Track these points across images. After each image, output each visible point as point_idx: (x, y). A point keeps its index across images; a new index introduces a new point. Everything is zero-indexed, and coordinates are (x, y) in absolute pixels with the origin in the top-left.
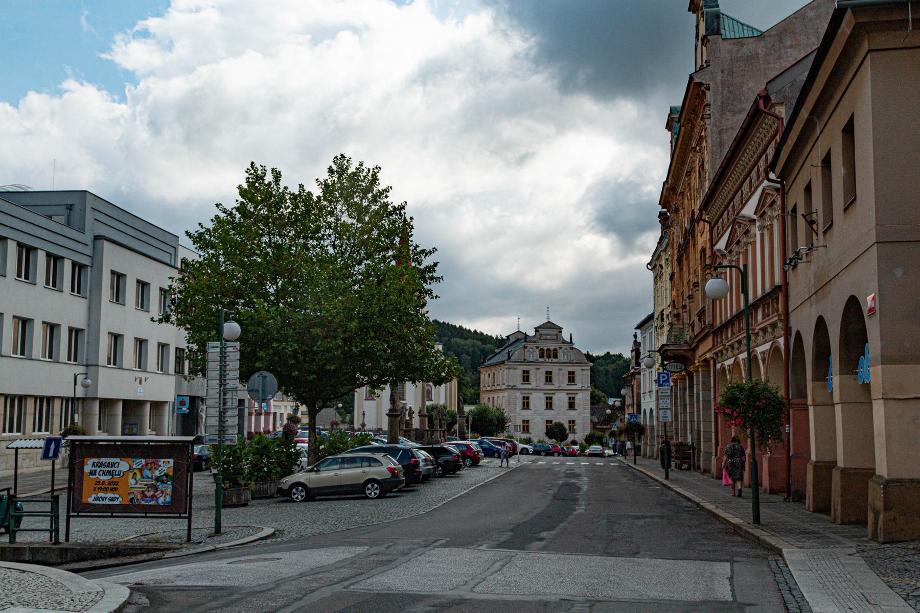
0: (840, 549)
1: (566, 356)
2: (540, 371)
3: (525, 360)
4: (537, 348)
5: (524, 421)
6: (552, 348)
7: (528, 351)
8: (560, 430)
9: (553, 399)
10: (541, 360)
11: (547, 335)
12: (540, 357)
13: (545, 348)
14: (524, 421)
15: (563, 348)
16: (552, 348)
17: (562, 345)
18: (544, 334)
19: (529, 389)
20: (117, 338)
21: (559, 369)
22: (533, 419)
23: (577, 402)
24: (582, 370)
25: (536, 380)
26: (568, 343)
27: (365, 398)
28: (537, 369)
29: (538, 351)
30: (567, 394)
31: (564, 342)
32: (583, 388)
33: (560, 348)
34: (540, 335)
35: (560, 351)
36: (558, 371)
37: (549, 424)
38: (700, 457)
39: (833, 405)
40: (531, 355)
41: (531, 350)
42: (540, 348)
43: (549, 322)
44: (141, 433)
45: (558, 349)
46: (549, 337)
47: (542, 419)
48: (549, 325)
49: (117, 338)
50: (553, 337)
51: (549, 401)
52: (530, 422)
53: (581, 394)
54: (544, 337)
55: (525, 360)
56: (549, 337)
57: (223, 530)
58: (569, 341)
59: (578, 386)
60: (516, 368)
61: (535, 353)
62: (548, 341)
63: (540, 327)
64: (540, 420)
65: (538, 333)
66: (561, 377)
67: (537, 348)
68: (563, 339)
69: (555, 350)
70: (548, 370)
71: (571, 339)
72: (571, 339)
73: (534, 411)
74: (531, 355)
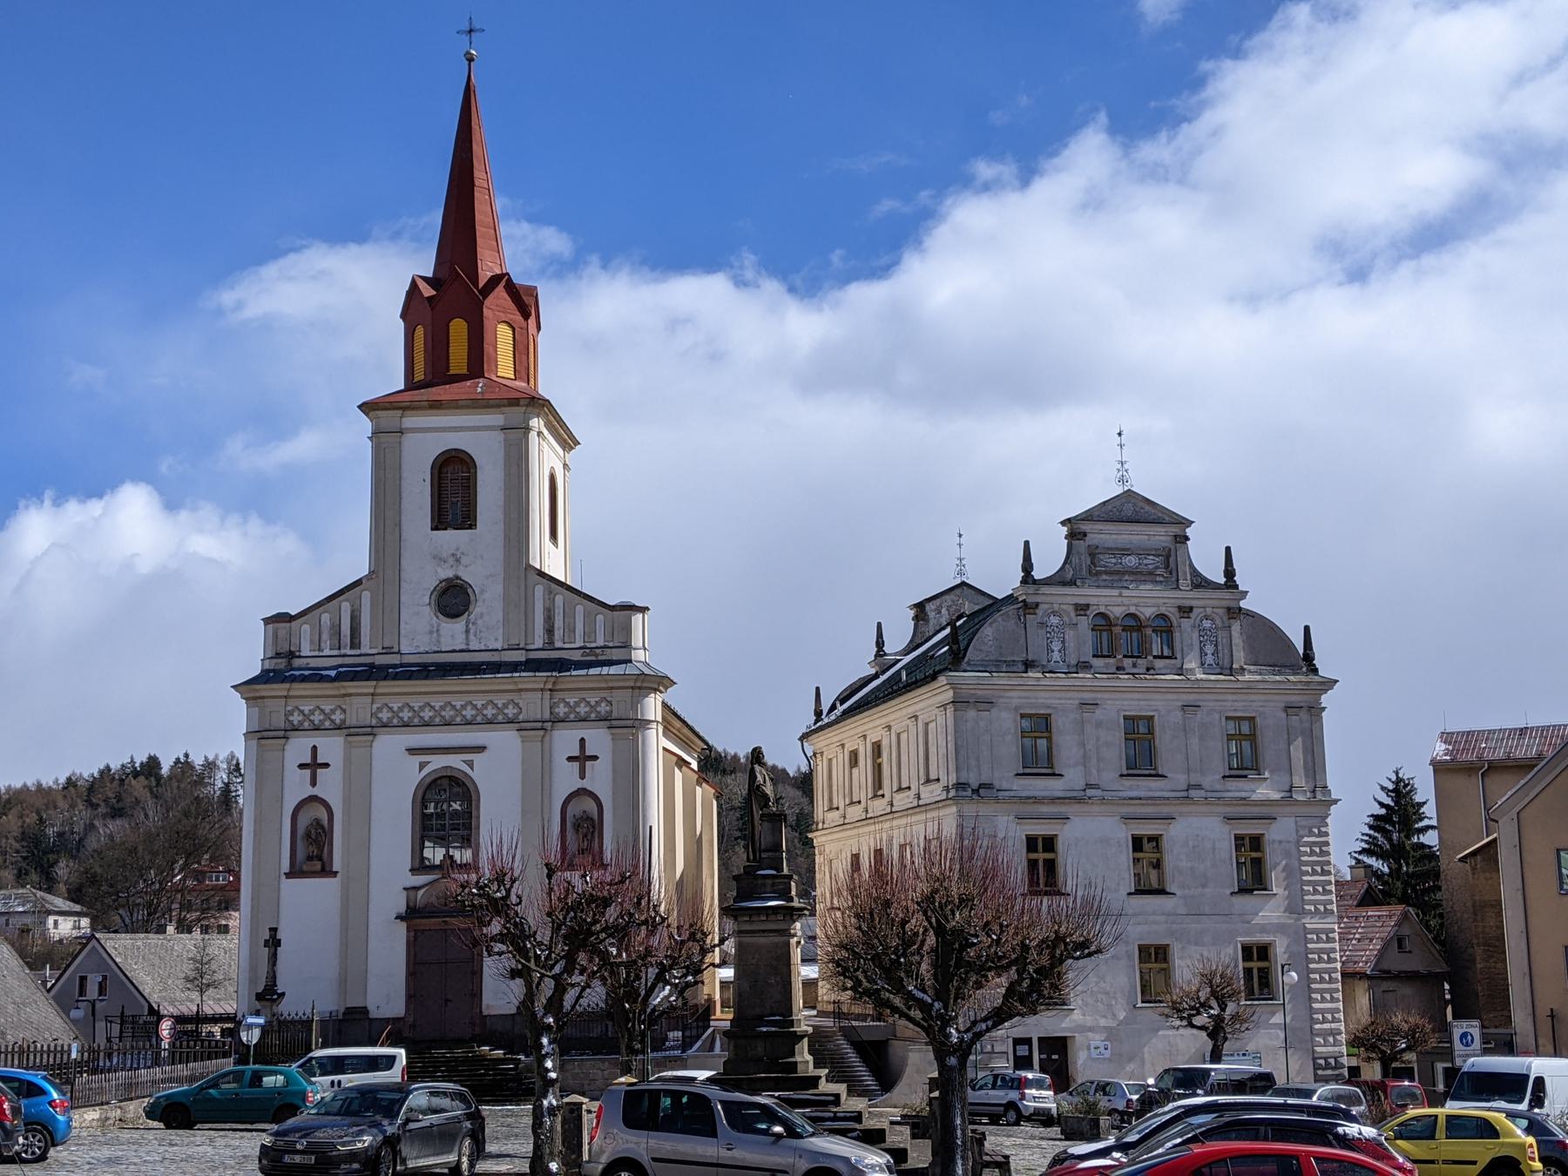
5: (1247, 951)
7: (1042, 624)
9: (1166, 844)
11: (1126, 551)
14: (1247, 951)
17: (1187, 595)
18: (1111, 551)
19: (1054, 800)
23: (1175, 858)
26: (1216, 586)
27: (286, 866)
29: (1084, 623)
30: (1127, 818)
31: (1200, 582)
34: (1093, 553)
35: (1186, 623)
38: (1169, 1141)
39: (339, 649)
40: (1056, 646)
41: (1054, 620)
43: (1129, 494)
44: (652, 1051)
46: (1131, 561)
48: (1129, 510)
51: (1041, 856)
58: (1222, 580)
59: (1073, 778)
61: (1070, 634)
63: (1088, 516)
65: (1081, 545)
66: (1194, 742)
67: (1082, 609)
68: (1195, 573)
71: (1230, 573)
72: (1230, 573)
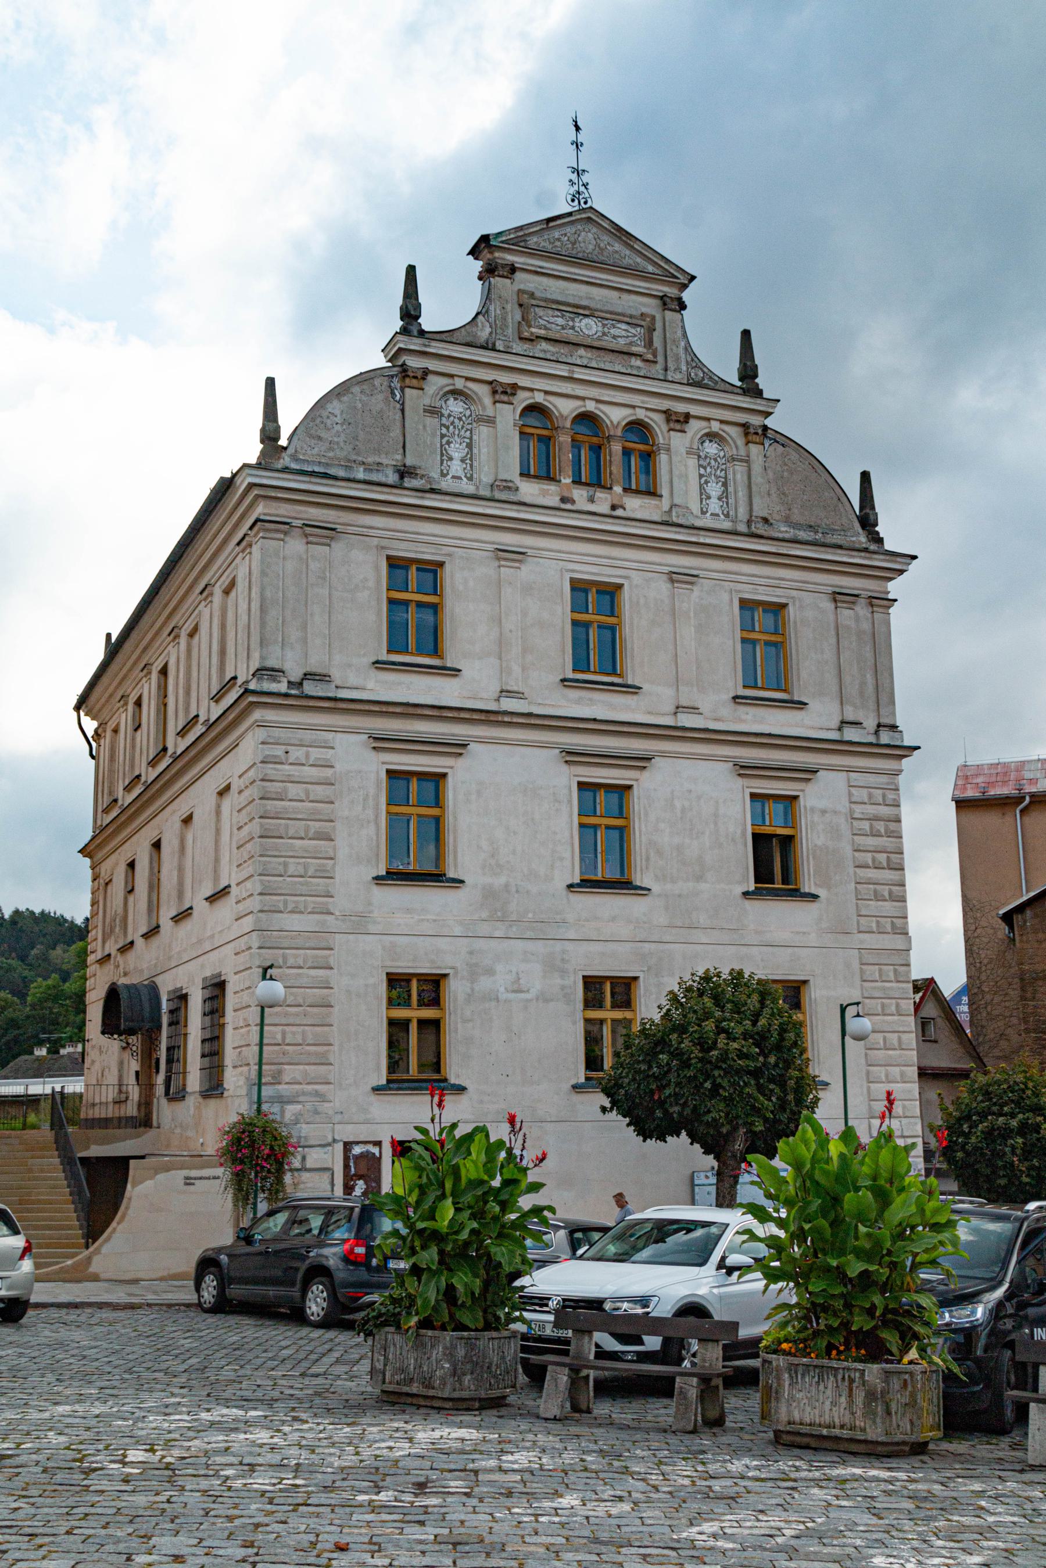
0: (120, 1227)
1: (714, 489)
2: (527, 571)
3: (404, 472)
4: (504, 392)
6: (616, 416)
7: (433, 411)
8: (760, 1039)
10: (530, 490)
12: (525, 474)
13: (565, 408)
15: (695, 427)
16: (616, 416)
19: (440, 712)
20: (724, 1367)
21: (673, 577)
22: (475, 972)
24: (837, 597)
25: (501, 645)
28: (502, 553)
29: (508, 416)
32: (851, 734)
33: (679, 421)
34: (526, 303)
35: (679, 442)
36: (662, 586)
37: (608, 1014)
40: (457, 451)
41: (455, 406)
42: (523, 399)
45: (657, 423)
46: (589, 327)
47: (553, 966)
49: (724, 1367)
50: (622, 335)
52: (455, 990)
53: (839, 780)
54: (555, 323)
55: (404, 472)
56: (589, 327)
57: (261, 970)
60: (330, 532)
62: (475, 464)
64: (536, 982)
66: (688, 633)
68: (694, 361)
69: (638, 428)
70: (587, 573)
73: (489, 894)
74: (457, 451)
